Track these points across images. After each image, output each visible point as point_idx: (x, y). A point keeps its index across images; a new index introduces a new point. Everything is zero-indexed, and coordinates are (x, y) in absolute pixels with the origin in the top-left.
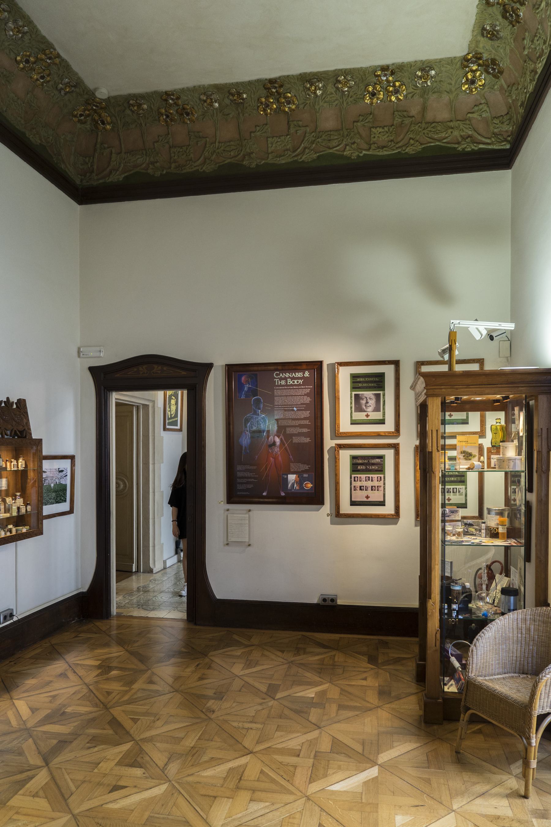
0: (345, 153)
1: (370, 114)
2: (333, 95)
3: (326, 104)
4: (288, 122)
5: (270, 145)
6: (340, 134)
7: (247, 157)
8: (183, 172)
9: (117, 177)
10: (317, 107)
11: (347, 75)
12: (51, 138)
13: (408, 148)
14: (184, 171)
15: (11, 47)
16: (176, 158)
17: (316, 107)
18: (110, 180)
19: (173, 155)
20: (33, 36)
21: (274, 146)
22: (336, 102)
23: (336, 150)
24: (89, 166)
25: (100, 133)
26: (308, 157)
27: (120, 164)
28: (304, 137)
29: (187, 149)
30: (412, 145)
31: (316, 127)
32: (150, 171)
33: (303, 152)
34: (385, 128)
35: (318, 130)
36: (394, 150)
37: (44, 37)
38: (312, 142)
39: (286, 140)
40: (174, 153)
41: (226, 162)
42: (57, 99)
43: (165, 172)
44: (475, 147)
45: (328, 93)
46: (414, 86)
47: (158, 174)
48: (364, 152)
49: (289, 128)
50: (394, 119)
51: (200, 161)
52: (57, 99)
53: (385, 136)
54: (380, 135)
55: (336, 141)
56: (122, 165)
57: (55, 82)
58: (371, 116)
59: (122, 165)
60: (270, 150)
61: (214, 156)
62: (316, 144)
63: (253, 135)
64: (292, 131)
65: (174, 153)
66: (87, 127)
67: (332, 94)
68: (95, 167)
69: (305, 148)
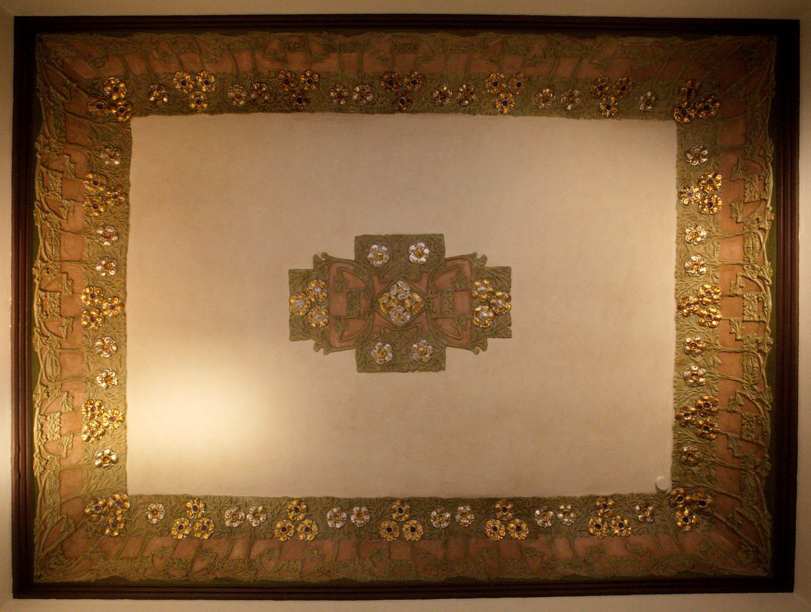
0: (767, 228)
1: (731, 206)
2: (707, 247)
3: (716, 254)
4: (730, 296)
5: (752, 319)
6: (748, 237)
7: (761, 348)
8: (770, 432)
9: (766, 520)
10: (718, 263)
11: (685, 233)
12: (686, 561)
13: (768, 155)
14: (769, 429)
15: (578, 529)
16: (753, 436)
17: (718, 265)
18: (769, 532)
19: (750, 439)
20: (578, 505)
21: (752, 314)
22: (715, 244)
23: (764, 239)
24: (751, 549)
25: (715, 514)
26: (768, 272)
27: (753, 509)
28: (747, 278)
29: (745, 419)
30: (765, 151)
31: (739, 264)
32: (765, 474)
33: (761, 278)
34: (746, 187)
35: (741, 262)
36: (769, 171)
37: (582, 498)
38: (754, 268)
39: (748, 298)
40: (748, 436)
41: (765, 375)
42: (653, 529)
43: (767, 456)
44: (773, 78)
45: (704, 252)
46: (707, 165)
47: (768, 465)
48: (768, 205)
49: (737, 295)
50: (738, 179)
51: (759, 406)
52: (653, 529)
53: (755, 184)
54: (753, 191)
55: (754, 241)
56: (755, 507)
57: (634, 519)
58: (733, 204)
59: (755, 507)
60: (757, 319)
61: (756, 388)
62: (756, 263)
63: (739, 337)
64: (739, 291)
65: (748, 436)
66: (705, 524)
67: (705, 248)
68: (753, 543)
69: (759, 277)
